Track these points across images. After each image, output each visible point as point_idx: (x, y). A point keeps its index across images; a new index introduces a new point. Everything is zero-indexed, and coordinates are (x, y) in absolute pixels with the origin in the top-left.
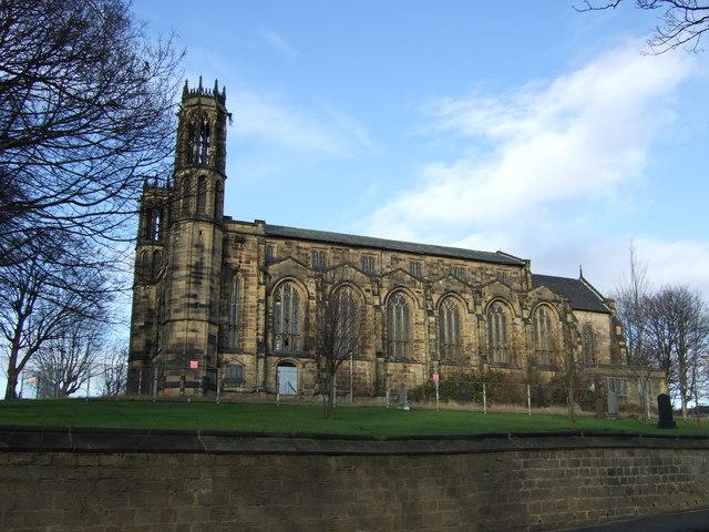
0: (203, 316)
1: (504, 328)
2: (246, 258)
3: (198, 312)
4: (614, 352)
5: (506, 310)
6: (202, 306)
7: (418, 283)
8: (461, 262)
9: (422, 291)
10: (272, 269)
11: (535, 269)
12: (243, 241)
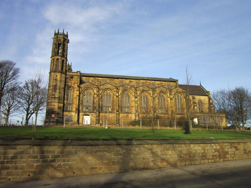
0: (57, 101)
1: (164, 101)
2: (74, 83)
3: (55, 100)
4: (209, 108)
5: (164, 95)
6: (56, 98)
7: (133, 88)
8: (153, 81)
9: (134, 91)
10: (82, 86)
11: (180, 83)
12: (72, 78)
